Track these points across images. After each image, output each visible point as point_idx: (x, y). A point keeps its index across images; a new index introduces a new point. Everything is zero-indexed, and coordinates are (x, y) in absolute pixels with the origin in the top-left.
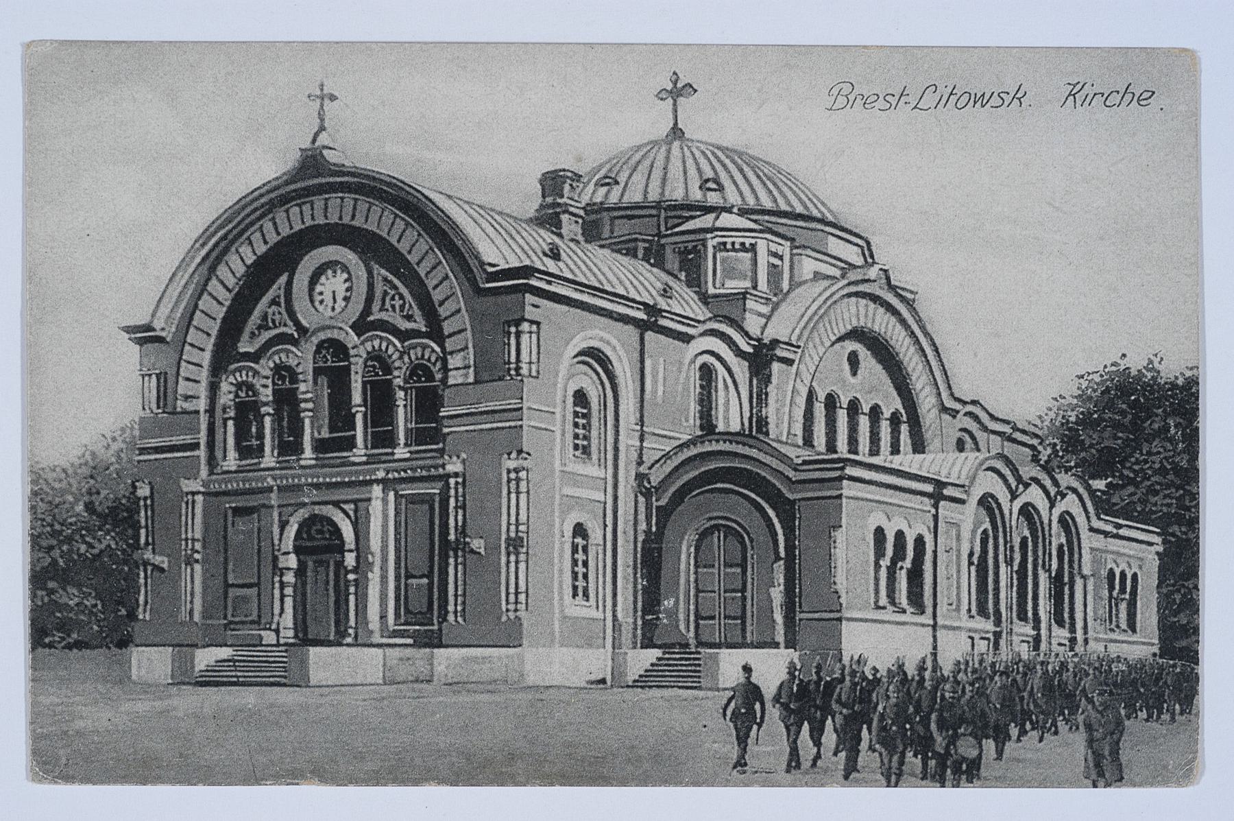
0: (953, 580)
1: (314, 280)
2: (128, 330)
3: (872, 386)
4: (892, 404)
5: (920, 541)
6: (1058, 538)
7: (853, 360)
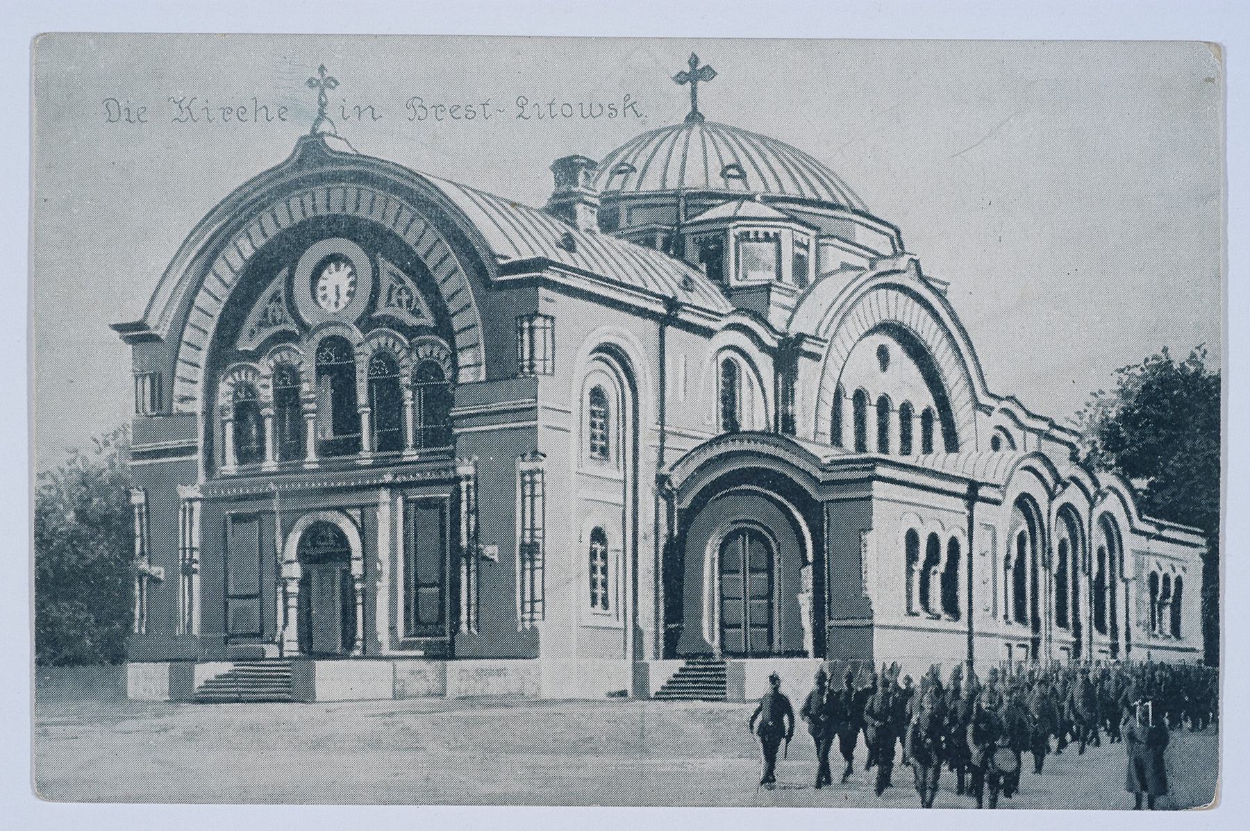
0: (987, 583)
1: (316, 275)
2: (118, 327)
3: (904, 383)
4: (923, 399)
5: (954, 544)
6: (1098, 539)
7: (883, 354)
